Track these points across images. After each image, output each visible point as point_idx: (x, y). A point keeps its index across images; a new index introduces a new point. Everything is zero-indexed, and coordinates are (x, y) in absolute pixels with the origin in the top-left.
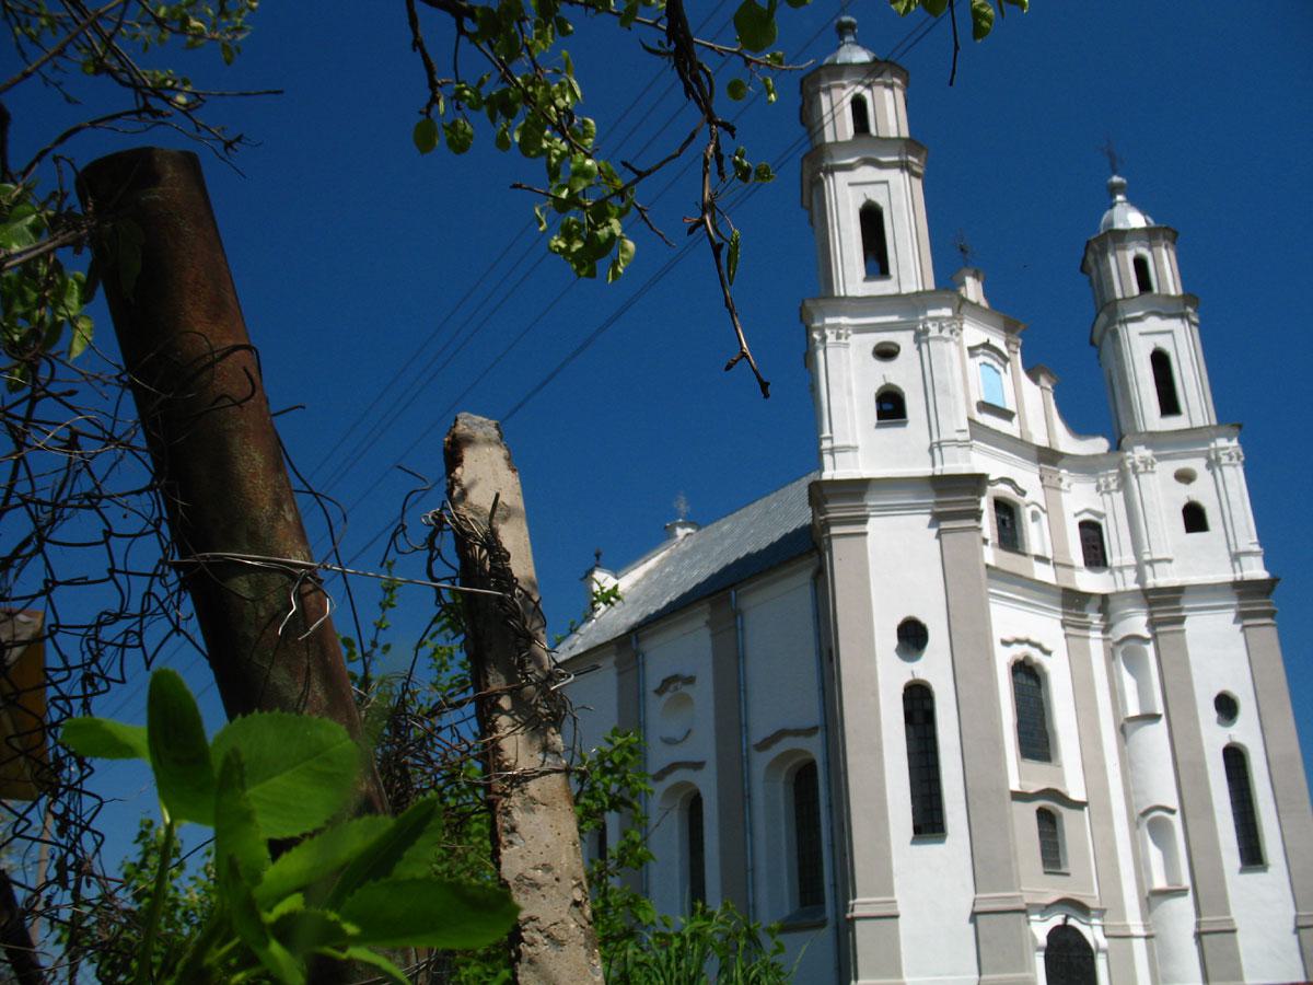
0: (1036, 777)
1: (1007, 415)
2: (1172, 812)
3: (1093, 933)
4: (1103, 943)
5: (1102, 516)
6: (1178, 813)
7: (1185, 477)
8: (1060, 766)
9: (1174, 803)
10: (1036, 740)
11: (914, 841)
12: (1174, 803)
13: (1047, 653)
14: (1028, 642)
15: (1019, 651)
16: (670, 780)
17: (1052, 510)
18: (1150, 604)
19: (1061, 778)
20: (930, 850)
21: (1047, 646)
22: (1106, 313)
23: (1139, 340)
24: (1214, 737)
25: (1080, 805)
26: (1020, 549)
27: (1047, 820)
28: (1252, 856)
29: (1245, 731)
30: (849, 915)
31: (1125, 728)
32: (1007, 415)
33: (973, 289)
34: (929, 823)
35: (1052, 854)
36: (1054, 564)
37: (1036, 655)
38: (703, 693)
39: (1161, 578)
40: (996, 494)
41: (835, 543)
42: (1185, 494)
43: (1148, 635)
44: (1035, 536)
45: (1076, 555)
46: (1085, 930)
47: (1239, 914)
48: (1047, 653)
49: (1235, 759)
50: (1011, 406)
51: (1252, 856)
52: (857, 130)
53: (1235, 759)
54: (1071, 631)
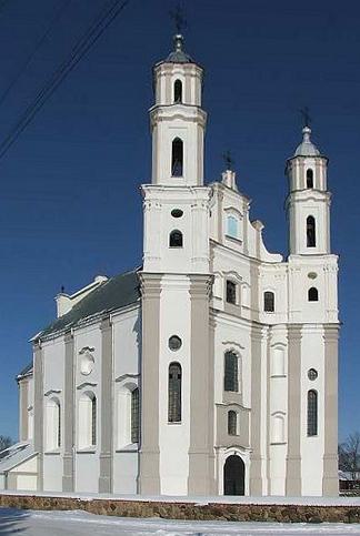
3: (245, 457)
7: (312, 276)
9: (286, 412)
10: (231, 383)
11: (310, 300)
15: (229, 347)
16: (84, 389)
20: (174, 426)
21: (242, 345)
22: (287, 191)
23: (301, 212)
24: (306, 385)
27: (232, 414)
28: (312, 431)
29: (318, 385)
30: (229, 177)
31: (270, 377)
33: (229, 177)
34: (175, 417)
35: (231, 429)
37: (237, 348)
38: (98, 354)
41: (159, 123)
44: (244, 295)
49: (313, 394)
52: (176, 100)
53: (313, 394)
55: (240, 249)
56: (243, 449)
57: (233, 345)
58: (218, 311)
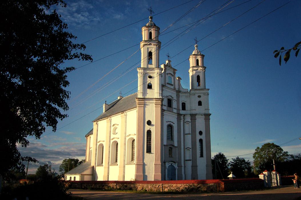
0: (170, 142)
1: (172, 85)
2: (190, 148)
3: (176, 166)
4: (177, 168)
5: (186, 102)
6: (191, 149)
7: (199, 97)
8: (174, 141)
9: (191, 147)
12: (191, 147)
13: (174, 123)
14: (171, 122)
15: (169, 123)
17: (178, 101)
18: (191, 116)
19: (174, 143)
28: (202, 156)
31: (184, 134)
32: (172, 85)
37: (172, 124)
39: (194, 112)
40: (169, 98)
42: (199, 99)
43: (190, 121)
45: (181, 108)
46: (175, 166)
47: (198, 164)
48: (174, 123)
49: (201, 141)
50: (173, 84)
51: (202, 156)
53: (201, 141)
54: (178, 120)
55: (172, 87)
56: (175, 162)
57: (170, 123)
58: (165, 110)
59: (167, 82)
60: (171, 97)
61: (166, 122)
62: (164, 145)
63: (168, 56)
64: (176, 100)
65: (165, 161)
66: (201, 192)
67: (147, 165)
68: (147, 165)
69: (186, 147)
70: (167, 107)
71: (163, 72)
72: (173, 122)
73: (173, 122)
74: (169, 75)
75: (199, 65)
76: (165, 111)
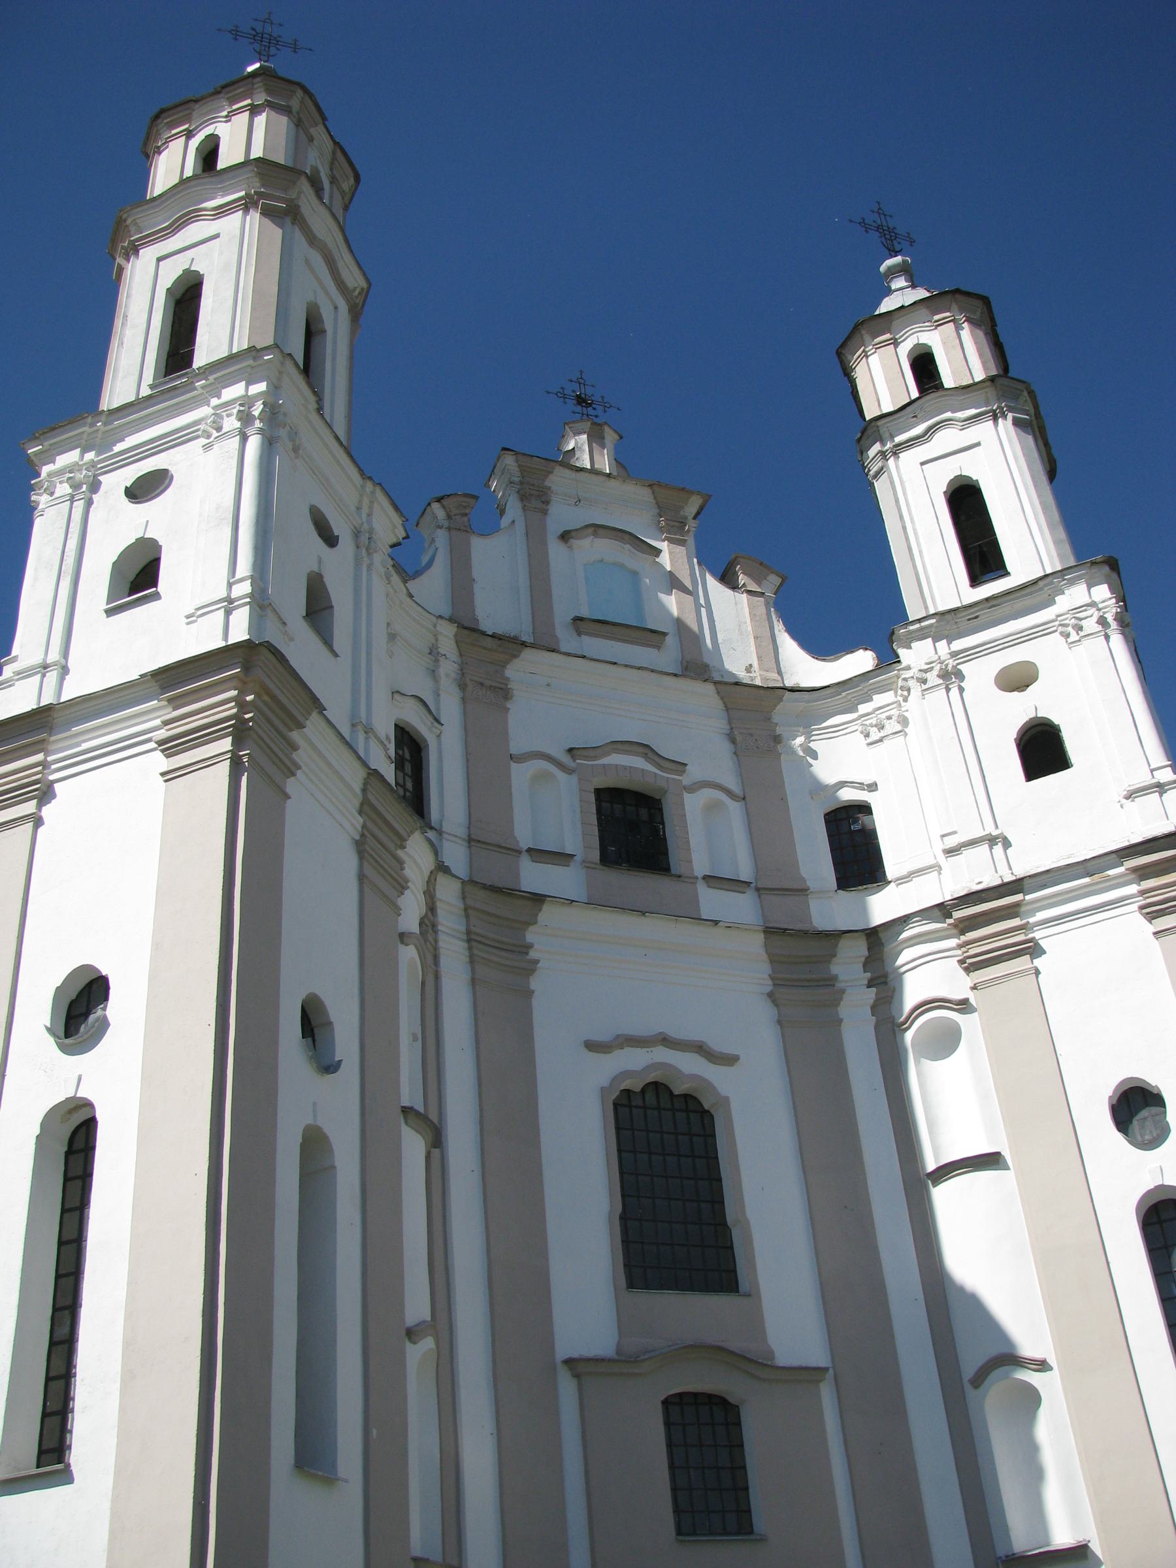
5: (872, 787)
8: (753, 1295)
13: (729, 1060)
14: (665, 1041)
19: (756, 1324)
21: (719, 1045)
25: (810, 1375)
26: (673, 871)
36: (758, 889)
37: (689, 1065)
48: (729, 1060)
57: (662, 1055)
59: (562, 614)
60: (638, 762)
61: (592, 1046)
62: (569, 1362)
63: (581, 401)
64: (732, 783)
65: (572, 389)
66: (668, 656)
67: (346, 1481)
68: (346, 1481)
69: (970, 1365)
70: (587, 865)
71: (80, 463)
72: (700, 1049)
73: (700, 1049)
74: (591, 548)
75: (939, 386)
76: (548, 914)
